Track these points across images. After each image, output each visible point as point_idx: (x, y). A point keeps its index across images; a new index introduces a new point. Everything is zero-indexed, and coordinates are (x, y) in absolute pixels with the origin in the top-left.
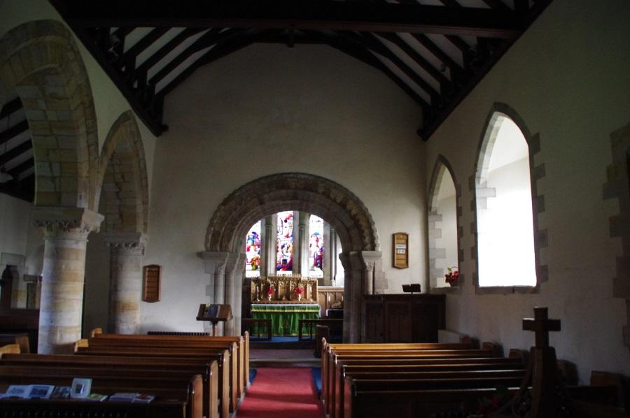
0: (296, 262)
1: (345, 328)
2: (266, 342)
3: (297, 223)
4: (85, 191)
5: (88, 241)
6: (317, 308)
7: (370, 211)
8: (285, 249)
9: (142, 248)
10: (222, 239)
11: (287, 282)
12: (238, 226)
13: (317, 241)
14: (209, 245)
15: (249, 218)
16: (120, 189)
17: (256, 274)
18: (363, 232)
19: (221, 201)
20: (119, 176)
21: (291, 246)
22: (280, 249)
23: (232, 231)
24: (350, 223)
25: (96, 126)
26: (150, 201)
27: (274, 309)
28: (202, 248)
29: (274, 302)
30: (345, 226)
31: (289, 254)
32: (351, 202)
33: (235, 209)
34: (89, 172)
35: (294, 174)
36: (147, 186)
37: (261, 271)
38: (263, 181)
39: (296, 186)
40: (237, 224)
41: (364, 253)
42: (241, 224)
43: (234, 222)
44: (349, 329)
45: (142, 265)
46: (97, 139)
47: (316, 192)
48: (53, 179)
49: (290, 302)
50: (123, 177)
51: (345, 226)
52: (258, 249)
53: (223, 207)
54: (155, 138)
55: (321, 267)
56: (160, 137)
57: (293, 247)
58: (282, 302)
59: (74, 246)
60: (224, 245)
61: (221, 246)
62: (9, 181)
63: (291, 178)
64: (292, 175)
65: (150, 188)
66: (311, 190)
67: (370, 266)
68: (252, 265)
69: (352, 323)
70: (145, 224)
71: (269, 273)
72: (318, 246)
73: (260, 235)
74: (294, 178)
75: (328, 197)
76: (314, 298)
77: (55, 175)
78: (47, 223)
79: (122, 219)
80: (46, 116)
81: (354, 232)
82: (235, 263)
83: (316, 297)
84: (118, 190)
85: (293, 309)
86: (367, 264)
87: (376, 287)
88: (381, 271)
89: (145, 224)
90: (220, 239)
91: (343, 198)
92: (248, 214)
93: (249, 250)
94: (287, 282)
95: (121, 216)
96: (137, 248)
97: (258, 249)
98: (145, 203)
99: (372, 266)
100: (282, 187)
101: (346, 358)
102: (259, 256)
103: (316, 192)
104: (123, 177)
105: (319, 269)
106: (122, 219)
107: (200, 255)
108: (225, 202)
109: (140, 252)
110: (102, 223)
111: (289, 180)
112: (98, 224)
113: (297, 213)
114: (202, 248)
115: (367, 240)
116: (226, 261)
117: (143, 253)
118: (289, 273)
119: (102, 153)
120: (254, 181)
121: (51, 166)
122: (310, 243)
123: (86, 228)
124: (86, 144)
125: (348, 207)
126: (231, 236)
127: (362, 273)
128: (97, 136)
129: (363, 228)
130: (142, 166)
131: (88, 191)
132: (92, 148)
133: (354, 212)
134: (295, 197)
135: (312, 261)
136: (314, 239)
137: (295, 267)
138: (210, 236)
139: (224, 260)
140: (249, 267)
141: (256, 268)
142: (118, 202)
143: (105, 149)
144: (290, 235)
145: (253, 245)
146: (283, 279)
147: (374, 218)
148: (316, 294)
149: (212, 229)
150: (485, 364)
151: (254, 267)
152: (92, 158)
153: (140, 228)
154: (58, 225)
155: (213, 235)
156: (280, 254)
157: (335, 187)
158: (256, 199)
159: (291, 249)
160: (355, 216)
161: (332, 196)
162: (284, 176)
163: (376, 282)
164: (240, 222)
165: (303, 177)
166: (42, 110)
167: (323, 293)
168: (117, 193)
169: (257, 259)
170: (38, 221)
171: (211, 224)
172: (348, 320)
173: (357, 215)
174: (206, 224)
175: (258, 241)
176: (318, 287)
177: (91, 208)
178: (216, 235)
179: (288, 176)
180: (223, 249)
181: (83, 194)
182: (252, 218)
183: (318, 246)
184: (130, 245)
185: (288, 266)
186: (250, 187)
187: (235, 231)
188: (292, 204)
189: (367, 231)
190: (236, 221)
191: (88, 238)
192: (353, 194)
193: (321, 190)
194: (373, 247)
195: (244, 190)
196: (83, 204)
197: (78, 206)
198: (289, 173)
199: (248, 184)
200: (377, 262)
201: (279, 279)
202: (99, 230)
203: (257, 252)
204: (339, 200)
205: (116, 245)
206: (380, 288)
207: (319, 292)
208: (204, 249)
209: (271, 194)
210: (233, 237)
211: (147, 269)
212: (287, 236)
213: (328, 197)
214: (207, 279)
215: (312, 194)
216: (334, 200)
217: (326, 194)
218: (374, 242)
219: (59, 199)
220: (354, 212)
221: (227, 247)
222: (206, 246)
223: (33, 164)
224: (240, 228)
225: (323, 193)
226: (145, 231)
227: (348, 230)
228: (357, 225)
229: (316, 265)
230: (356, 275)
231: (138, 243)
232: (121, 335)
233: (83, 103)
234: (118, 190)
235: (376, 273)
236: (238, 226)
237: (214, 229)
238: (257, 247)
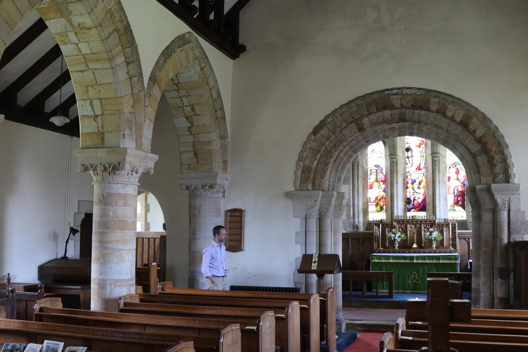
0: (429, 201)
1: (473, 286)
2: (386, 299)
3: (429, 152)
4: (130, 129)
5: (139, 184)
6: (456, 258)
7: (503, 130)
8: (416, 185)
9: (222, 190)
10: (315, 175)
11: (418, 226)
12: (333, 159)
13: (457, 172)
14: (298, 183)
15: (347, 148)
16: (192, 124)
17: (382, 216)
18: (493, 158)
19: (311, 130)
20: (189, 109)
21: (424, 180)
22: (410, 185)
23: (327, 165)
24: (475, 148)
25: (138, 54)
26: (229, 135)
27: (381, 259)
28: (291, 188)
29: (402, 250)
30: (470, 152)
31: (422, 191)
32: (475, 120)
33: (328, 139)
34: (133, 107)
35: (399, 89)
36: (224, 118)
37: (386, 212)
38: (360, 102)
39: (401, 104)
40: (331, 157)
41: (494, 186)
42: (338, 156)
43: (328, 154)
44: (478, 285)
45: (223, 210)
46: (141, 69)
47: (428, 110)
48: (96, 117)
49: (422, 250)
50: (193, 109)
51: (470, 152)
52: (383, 186)
53: (313, 137)
54: (231, 61)
55: (463, 206)
56: (237, 59)
57: (427, 182)
58: (412, 251)
59: (122, 191)
60: (317, 183)
61: (313, 186)
62: (66, 124)
63: (394, 94)
64: (395, 91)
65: (228, 118)
66: (421, 108)
67: (504, 204)
68: (377, 205)
69: (482, 279)
70: (225, 162)
71: (395, 214)
72: (458, 179)
73: (384, 169)
74: (397, 94)
75: (444, 114)
76: (454, 246)
77: (97, 113)
78: (92, 167)
79: (197, 158)
80: (79, 50)
81: (482, 159)
82: (330, 204)
83: (455, 245)
84: (189, 125)
85: (389, 259)
86: (499, 201)
87: (512, 231)
88: (519, 210)
89: (225, 162)
90: (312, 176)
91: (464, 116)
92: (345, 143)
93: (371, 187)
94: (418, 226)
95: (196, 154)
96: (215, 190)
97: (383, 186)
98: (223, 138)
99: (506, 203)
100: (385, 108)
101: (411, 324)
102: (384, 194)
103: (428, 110)
104: (193, 109)
105: (461, 209)
106: (197, 158)
107: (288, 195)
108: (316, 131)
109: (220, 195)
110: (156, 164)
111: (392, 97)
112: (151, 165)
113: (429, 142)
114: (291, 188)
115: (499, 168)
116: (318, 202)
117: (224, 197)
118: (421, 215)
119: (149, 84)
120: (349, 103)
121: (91, 104)
122: (448, 175)
123: (134, 170)
124: (126, 76)
125: (471, 127)
126: (325, 172)
127: (493, 212)
128: (140, 66)
129: (492, 154)
130: (215, 96)
131: (134, 129)
132: (135, 79)
133: (479, 133)
134: (402, 119)
135: (451, 199)
136: (453, 170)
137: (429, 207)
138: (299, 173)
139: (316, 201)
140: (372, 208)
141: (382, 209)
142: (191, 139)
143: (153, 79)
144: (421, 167)
145: (377, 181)
146: (414, 221)
147: (508, 140)
148: (455, 241)
149: (302, 164)
150: (325, 337)
151: (378, 208)
152: (135, 91)
153: (217, 166)
154: (103, 168)
155: (303, 172)
156: (410, 190)
157: (452, 102)
158: (353, 125)
159: (423, 184)
160: (481, 138)
161: (449, 113)
162: (386, 92)
163: (305, 222)
164: (336, 154)
165: (409, 92)
166: (74, 44)
167: (465, 239)
168: (189, 128)
169: (382, 198)
170: (83, 165)
171: (301, 159)
172: (478, 275)
173: (483, 136)
174: (296, 157)
175: (381, 176)
176: (457, 231)
177: (139, 147)
178: (306, 170)
179: (390, 92)
180: (317, 188)
181: (127, 132)
182: (351, 148)
183: (458, 179)
184: (207, 187)
185: (422, 207)
186: (344, 110)
187: (330, 165)
188: (400, 128)
189: (497, 157)
190: (330, 152)
191: (139, 182)
192: (476, 109)
193: (434, 107)
194: (507, 179)
195: (337, 114)
196: (129, 144)
197: (122, 146)
198: (392, 89)
199: (341, 107)
200: (514, 198)
201: (408, 222)
202: (152, 172)
203: (382, 190)
204: (458, 118)
205: (192, 188)
206: (519, 233)
207: (460, 238)
208: (293, 189)
209: (372, 117)
210: (328, 172)
211: (229, 214)
212: (419, 169)
213: (444, 114)
214: (296, 225)
215: (423, 112)
216: (452, 119)
217: (442, 112)
218: (508, 172)
219: (103, 139)
220: (479, 133)
221: (320, 185)
222: (295, 185)
223: (75, 102)
224: (338, 161)
225: (438, 111)
226: (225, 169)
227: (474, 156)
228: (485, 150)
229: (456, 203)
230: (487, 216)
231: (216, 184)
232: (203, 290)
233: (117, 30)
234: (189, 125)
235: (511, 213)
236: (333, 159)
237: (304, 165)
238: (381, 183)
